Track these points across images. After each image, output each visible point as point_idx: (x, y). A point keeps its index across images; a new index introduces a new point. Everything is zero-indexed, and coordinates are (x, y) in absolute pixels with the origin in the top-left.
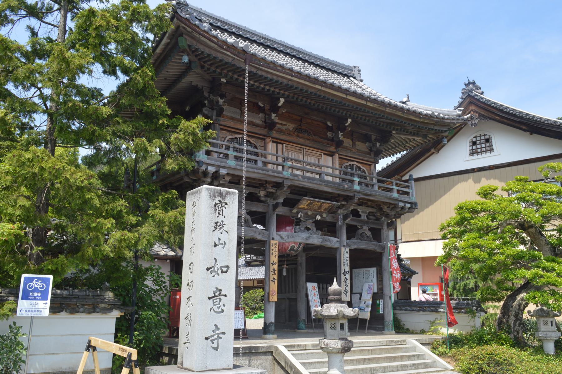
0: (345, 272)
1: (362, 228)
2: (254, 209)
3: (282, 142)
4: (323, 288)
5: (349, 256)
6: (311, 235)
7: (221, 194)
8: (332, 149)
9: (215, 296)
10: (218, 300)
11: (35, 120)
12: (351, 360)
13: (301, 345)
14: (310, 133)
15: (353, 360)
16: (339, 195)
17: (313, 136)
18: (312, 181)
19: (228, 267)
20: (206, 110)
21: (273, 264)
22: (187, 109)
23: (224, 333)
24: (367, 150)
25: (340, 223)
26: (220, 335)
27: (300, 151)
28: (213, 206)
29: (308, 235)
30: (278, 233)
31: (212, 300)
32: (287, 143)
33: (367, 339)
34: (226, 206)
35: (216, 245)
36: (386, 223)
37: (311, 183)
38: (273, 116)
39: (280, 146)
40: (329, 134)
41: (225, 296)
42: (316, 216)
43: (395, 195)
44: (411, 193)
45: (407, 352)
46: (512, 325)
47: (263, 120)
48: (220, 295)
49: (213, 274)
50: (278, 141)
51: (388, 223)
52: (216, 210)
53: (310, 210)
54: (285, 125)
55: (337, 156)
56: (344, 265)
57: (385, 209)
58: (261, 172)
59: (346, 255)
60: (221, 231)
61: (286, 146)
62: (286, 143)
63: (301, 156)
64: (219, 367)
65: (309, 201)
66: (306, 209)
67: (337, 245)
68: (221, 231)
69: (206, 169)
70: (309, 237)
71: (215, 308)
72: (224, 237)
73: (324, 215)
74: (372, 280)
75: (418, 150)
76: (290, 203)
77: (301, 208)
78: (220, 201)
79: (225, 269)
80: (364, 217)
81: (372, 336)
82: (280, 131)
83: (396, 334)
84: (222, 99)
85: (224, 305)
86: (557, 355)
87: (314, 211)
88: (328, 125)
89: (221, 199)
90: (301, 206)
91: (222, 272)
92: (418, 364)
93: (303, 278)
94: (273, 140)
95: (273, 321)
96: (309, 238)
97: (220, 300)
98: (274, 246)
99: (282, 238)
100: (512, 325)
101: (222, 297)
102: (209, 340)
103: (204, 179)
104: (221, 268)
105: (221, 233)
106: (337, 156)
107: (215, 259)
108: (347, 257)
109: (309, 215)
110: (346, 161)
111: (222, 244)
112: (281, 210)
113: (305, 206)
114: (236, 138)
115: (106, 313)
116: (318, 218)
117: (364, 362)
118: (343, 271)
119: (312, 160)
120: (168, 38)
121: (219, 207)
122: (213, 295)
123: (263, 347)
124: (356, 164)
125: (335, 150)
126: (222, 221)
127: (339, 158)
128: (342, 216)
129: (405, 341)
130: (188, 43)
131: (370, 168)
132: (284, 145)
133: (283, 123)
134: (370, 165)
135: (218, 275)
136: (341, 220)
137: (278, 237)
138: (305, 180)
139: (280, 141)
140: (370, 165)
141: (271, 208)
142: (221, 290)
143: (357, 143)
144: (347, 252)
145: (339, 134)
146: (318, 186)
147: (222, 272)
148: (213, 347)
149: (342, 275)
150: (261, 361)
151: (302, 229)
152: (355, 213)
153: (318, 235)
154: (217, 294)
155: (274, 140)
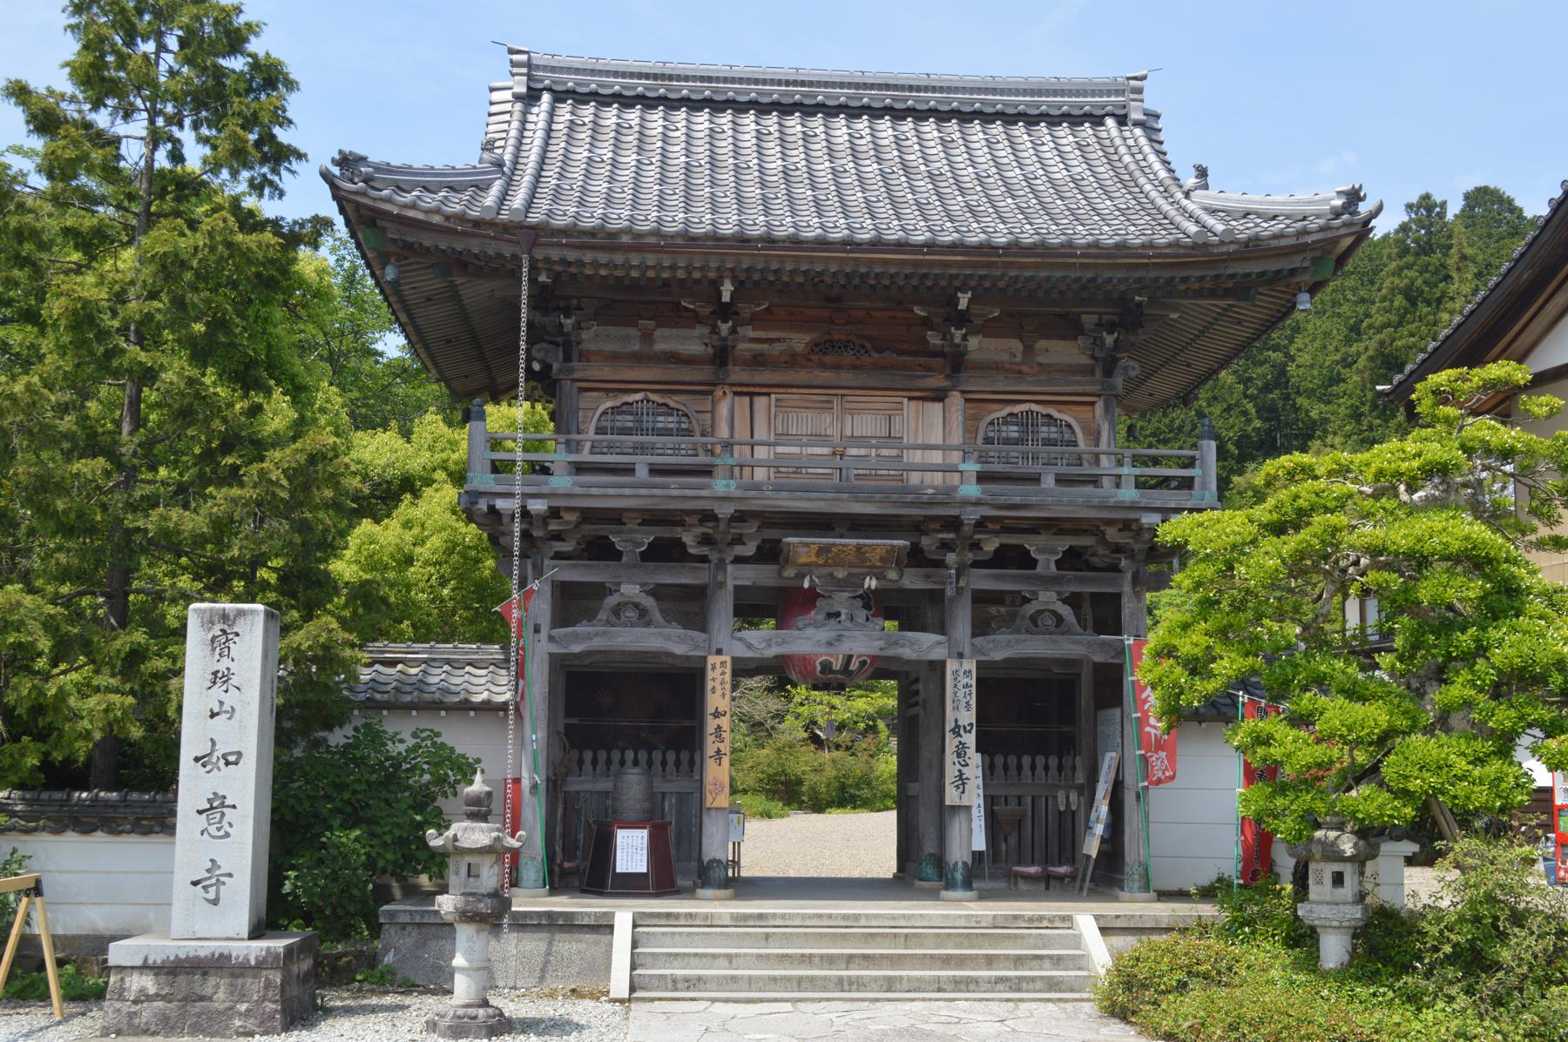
0: (957, 726)
2: (667, 578)
4: (1006, 768)
8: (936, 381)
9: (212, 808)
10: (218, 815)
12: (803, 955)
13: (696, 914)
14: (862, 347)
15: (811, 956)
17: (875, 355)
18: (806, 495)
19: (239, 754)
20: (539, 350)
21: (717, 714)
23: (230, 875)
26: (222, 879)
27: (826, 407)
29: (833, 634)
31: (205, 815)
32: (781, 390)
33: (893, 908)
34: (236, 639)
35: (213, 715)
37: (801, 499)
39: (761, 402)
41: (234, 807)
43: (1129, 494)
45: (1044, 948)
49: (208, 768)
52: (214, 649)
54: (778, 340)
55: (956, 400)
56: (956, 708)
58: (643, 492)
60: (224, 688)
61: (777, 400)
64: (218, 935)
66: (823, 566)
67: (938, 654)
68: (224, 688)
70: (839, 638)
71: (213, 830)
72: (231, 699)
73: (892, 575)
75: (1523, 272)
77: (805, 565)
78: (223, 631)
79: (232, 758)
80: (1046, 564)
81: (996, 903)
82: (758, 361)
83: (1159, 901)
84: (567, 316)
85: (231, 825)
86: (5, 895)
89: (226, 627)
91: (227, 763)
92: (1020, 978)
94: (734, 389)
95: (1094, 854)
96: (839, 640)
97: (223, 814)
98: (719, 670)
99: (750, 646)
101: (225, 810)
104: (224, 756)
107: (212, 740)
108: (967, 686)
109: (839, 580)
110: (995, 406)
111: (227, 712)
113: (814, 559)
116: (871, 583)
118: (949, 725)
119: (867, 424)
121: (221, 643)
122: (208, 806)
123: (588, 914)
124: (1035, 407)
125: (945, 383)
126: (228, 669)
127: (967, 400)
129: (1064, 919)
133: (773, 335)
134: (1093, 404)
135: (219, 769)
138: (784, 494)
139: (757, 390)
140: (1093, 404)
142: (225, 797)
143: (1042, 344)
144: (968, 673)
147: (227, 763)
148: (208, 900)
149: (949, 736)
150: (582, 946)
151: (821, 617)
153: (874, 630)
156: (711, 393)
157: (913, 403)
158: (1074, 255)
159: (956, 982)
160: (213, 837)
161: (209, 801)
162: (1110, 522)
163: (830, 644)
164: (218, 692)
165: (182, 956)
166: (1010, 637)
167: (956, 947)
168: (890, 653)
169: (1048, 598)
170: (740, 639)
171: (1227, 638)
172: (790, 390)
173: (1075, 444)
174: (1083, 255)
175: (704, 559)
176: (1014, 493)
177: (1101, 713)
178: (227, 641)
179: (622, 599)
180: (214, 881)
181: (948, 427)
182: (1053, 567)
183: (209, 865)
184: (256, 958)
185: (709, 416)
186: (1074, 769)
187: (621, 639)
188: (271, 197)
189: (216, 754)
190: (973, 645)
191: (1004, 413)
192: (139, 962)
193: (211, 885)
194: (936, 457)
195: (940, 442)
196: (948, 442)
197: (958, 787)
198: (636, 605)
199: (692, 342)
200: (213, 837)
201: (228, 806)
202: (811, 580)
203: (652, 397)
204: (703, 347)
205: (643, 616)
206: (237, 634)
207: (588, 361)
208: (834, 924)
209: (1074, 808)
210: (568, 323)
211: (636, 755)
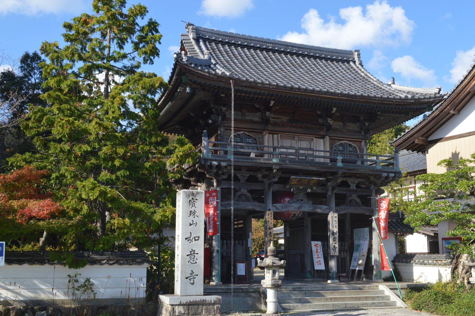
1: (351, 196)
3: (277, 133)
5: (337, 220)
6: (303, 205)
7: (193, 194)
8: (323, 133)
9: (191, 254)
10: (193, 256)
11: (145, 8)
14: (302, 122)
16: (325, 172)
19: (199, 237)
22: (204, 113)
23: (197, 275)
24: (358, 129)
25: (329, 193)
26: (195, 277)
27: (293, 138)
28: (188, 202)
29: (300, 205)
30: (274, 205)
31: (189, 256)
32: (282, 133)
34: (197, 201)
35: (190, 225)
36: (374, 190)
38: (268, 114)
39: (275, 136)
40: (320, 121)
41: (198, 254)
42: (307, 189)
44: (395, 164)
45: (376, 294)
46: (460, 273)
47: (261, 117)
48: (194, 253)
50: (274, 132)
51: (376, 190)
52: (190, 204)
53: (301, 185)
54: (279, 118)
55: (327, 138)
57: (372, 178)
59: (335, 219)
60: (194, 216)
61: (280, 136)
62: (280, 133)
63: (294, 142)
65: (298, 179)
66: (297, 185)
68: (194, 216)
69: (211, 164)
70: (301, 206)
73: (315, 188)
74: (366, 238)
76: (284, 181)
78: (193, 198)
79: (197, 238)
80: (353, 187)
82: (275, 124)
84: (224, 107)
85: (197, 259)
87: (304, 185)
88: (318, 114)
90: (293, 183)
91: (195, 240)
93: (309, 237)
94: (269, 132)
99: (277, 208)
100: (460, 273)
101: (195, 255)
102: (188, 279)
103: (211, 170)
104: (194, 238)
105: (194, 217)
106: (327, 138)
107: (190, 233)
108: (335, 221)
109: (301, 189)
110: (337, 141)
112: (276, 187)
113: (296, 183)
114: (238, 134)
115: (140, 265)
116: (309, 190)
117: (331, 300)
119: (304, 144)
120: (176, 76)
122: (190, 254)
124: (347, 142)
127: (330, 139)
128: (331, 188)
130: (189, 78)
131: (361, 144)
132: (279, 135)
133: (278, 117)
136: (330, 191)
137: (274, 208)
140: (361, 142)
141: (267, 186)
142: (194, 251)
143: (348, 124)
144: (335, 217)
145: (328, 120)
146: (304, 167)
147: (195, 240)
148: (190, 283)
151: (295, 200)
152: (344, 184)
154: (192, 253)
155: (270, 132)
156: (262, 133)
157: (316, 139)
158: (376, 100)
159: (362, 304)
160: (192, 263)
161: (191, 252)
162: (372, 175)
163: (299, 208)
164: (192, 217)
165: (192, 301)
166: (345, 207)
167: (354, 295)
168: (314, 211)
169: (354, 197)
170: (274, 206)
171: (466, 206)
172: (284, 133)
173: (357, 152)
174: (379, 100)
175: (262, 182)
176: (351, 166)
177: (355, 230)
178: (194, 202)
179: (241, 194)
180: (192, 277)
181: (325, 146)
182: (355, 187)
183: (191, 272)
184: (214, 301)
185: (261, 139)
186: (345, 245)
187: (241, 206)
188: (150, 64)
189: (192, 237)
190: (336, 209)
191: (339, 143)
192: (178, 303)
193: (192, 279)
194: (322, 154)
195: (323, 150)
196: (325, 150)
197: (334, 250)
198: (245, 195)
199: (256, 117)
200: (192, 263)
201: (196, 254)
202: (293, 189)
203: (246, 133)
204: (259, 119)
205: (247, 200)
206: (197, 200)
207: (227, 121)
208: (319, 289)
209: (345, 257)
210: (224, 109)
211: (227, 242)
